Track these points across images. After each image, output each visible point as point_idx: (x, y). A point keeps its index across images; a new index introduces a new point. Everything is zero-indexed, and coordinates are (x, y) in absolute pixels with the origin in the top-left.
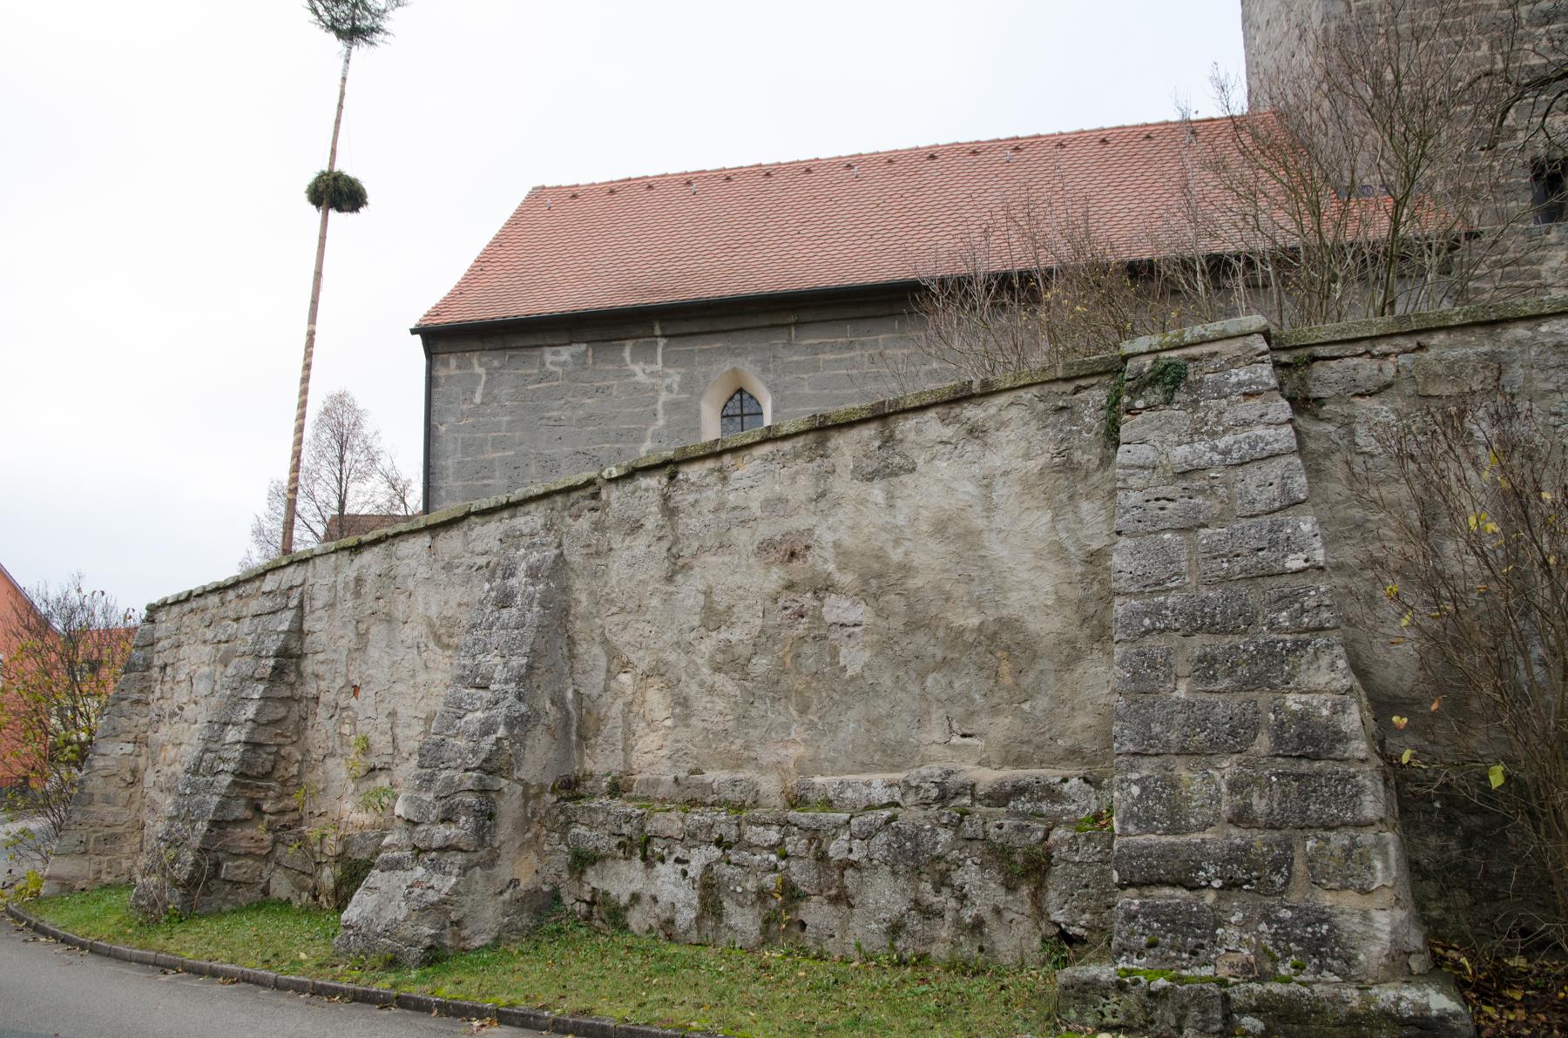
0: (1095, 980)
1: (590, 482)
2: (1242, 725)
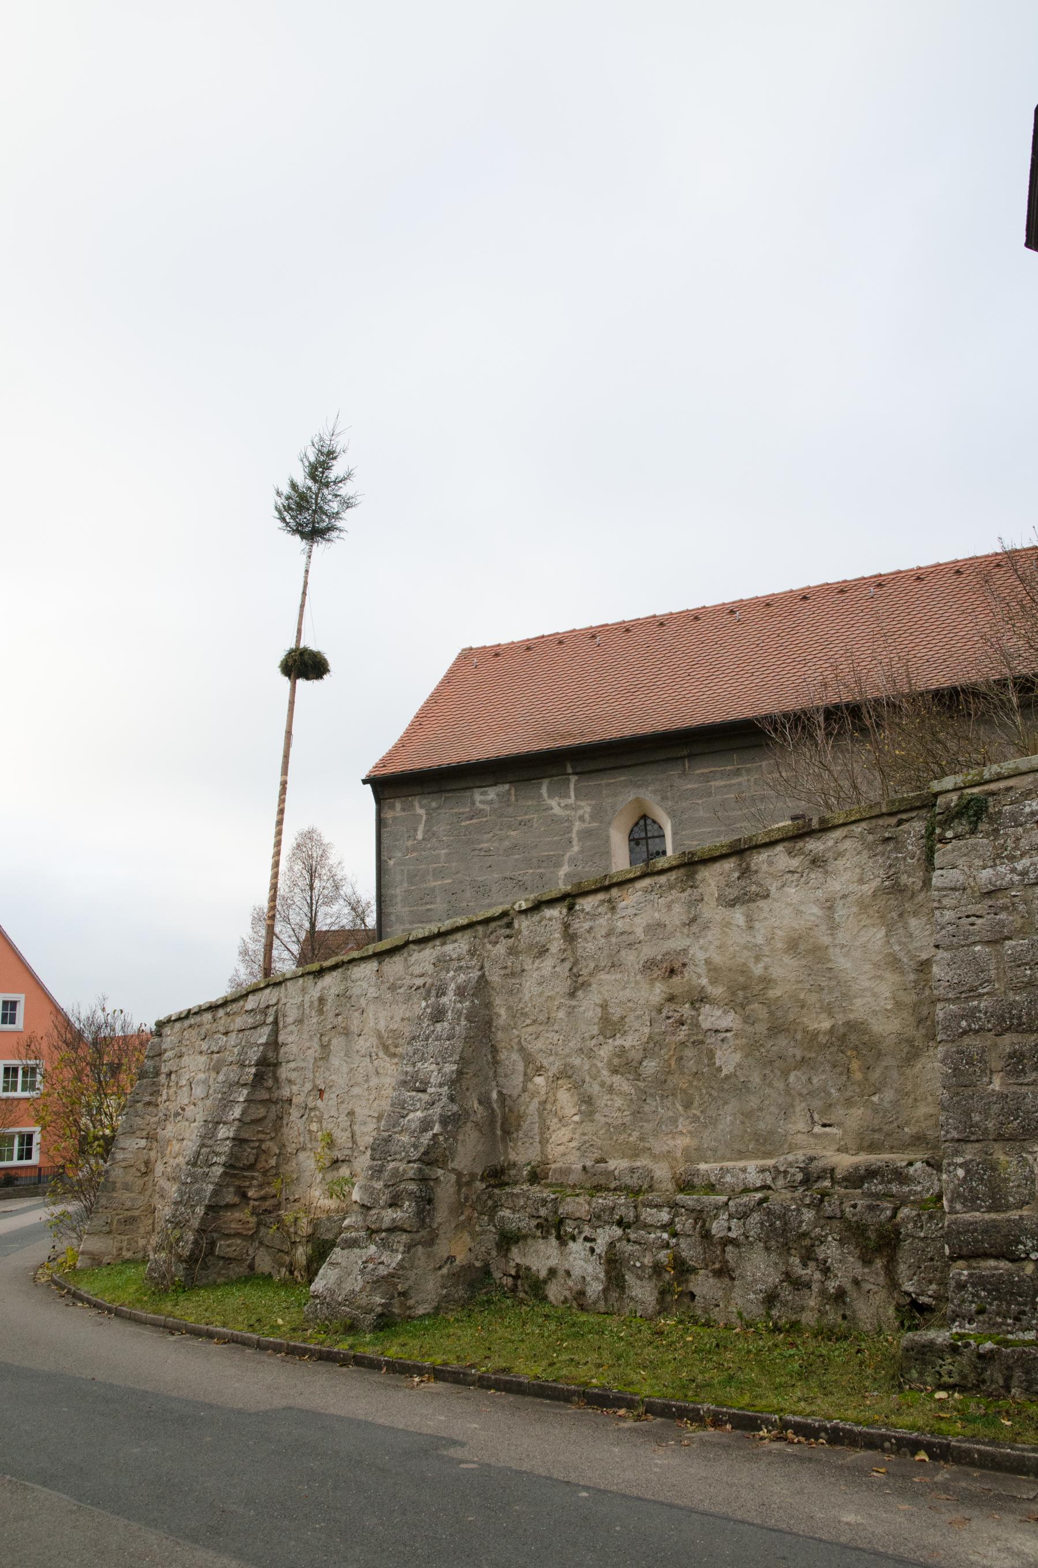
0: (932, 1343)
1: (504, 914)
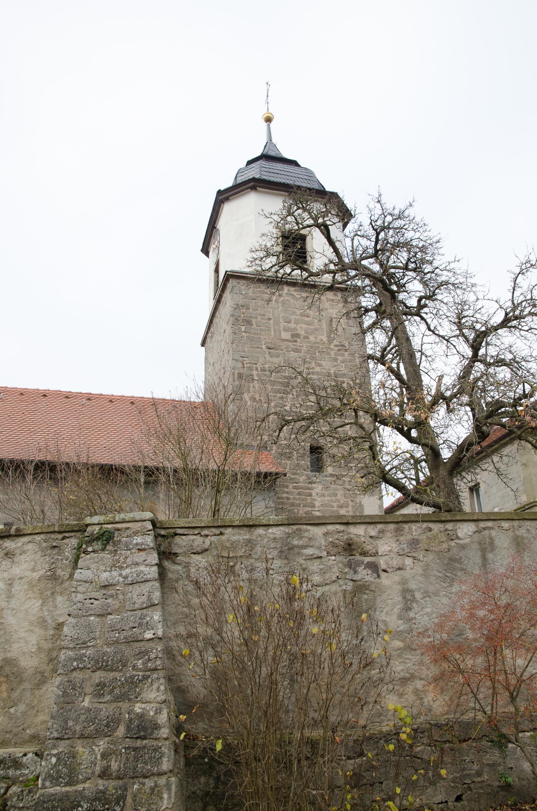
2: (112, 721)
